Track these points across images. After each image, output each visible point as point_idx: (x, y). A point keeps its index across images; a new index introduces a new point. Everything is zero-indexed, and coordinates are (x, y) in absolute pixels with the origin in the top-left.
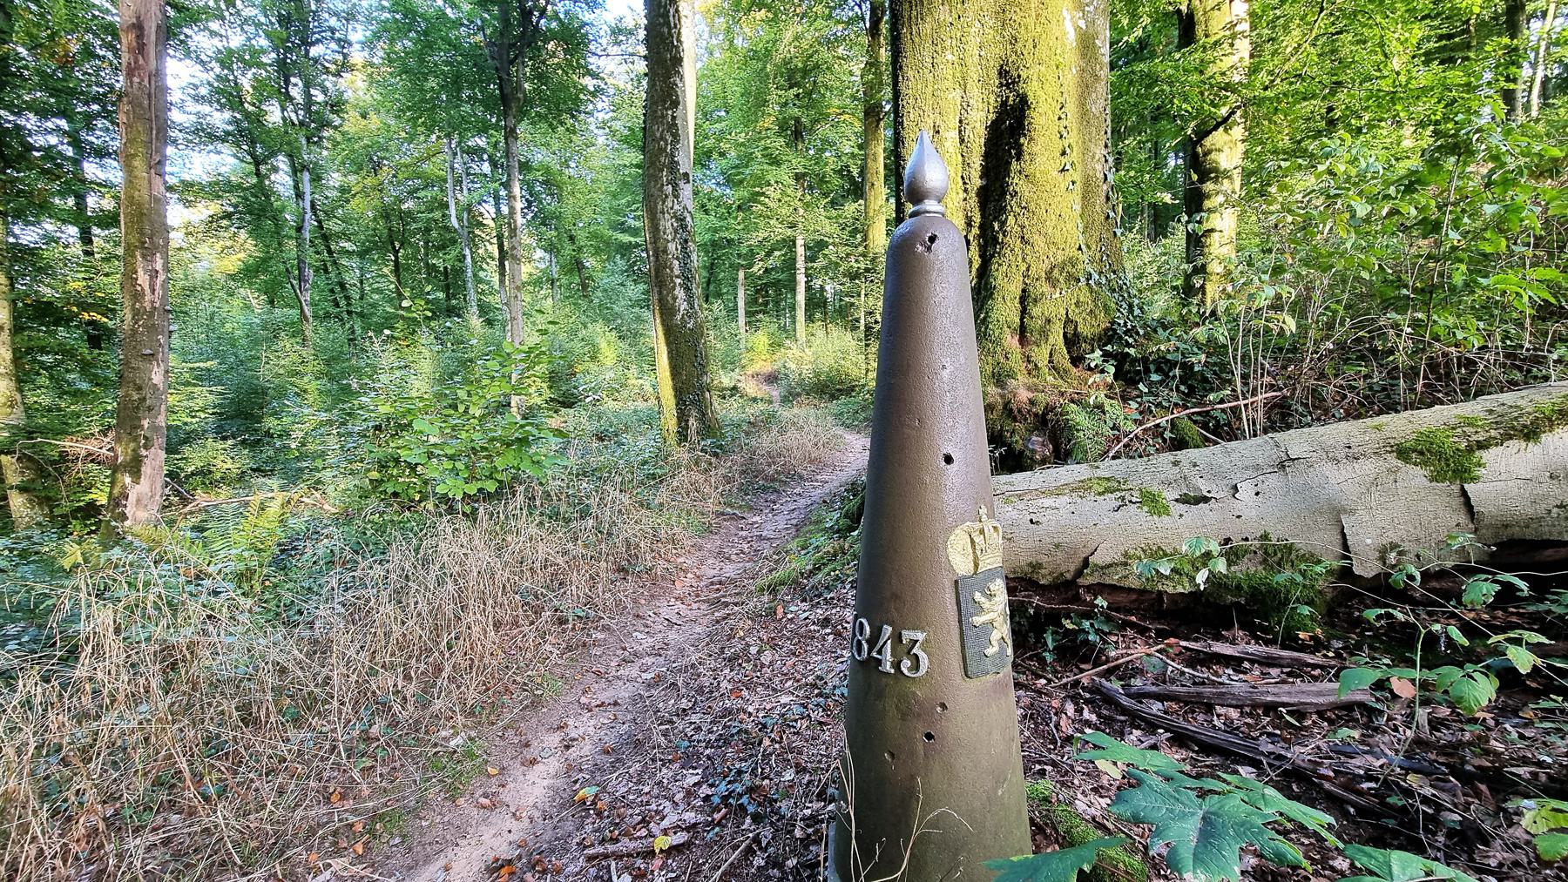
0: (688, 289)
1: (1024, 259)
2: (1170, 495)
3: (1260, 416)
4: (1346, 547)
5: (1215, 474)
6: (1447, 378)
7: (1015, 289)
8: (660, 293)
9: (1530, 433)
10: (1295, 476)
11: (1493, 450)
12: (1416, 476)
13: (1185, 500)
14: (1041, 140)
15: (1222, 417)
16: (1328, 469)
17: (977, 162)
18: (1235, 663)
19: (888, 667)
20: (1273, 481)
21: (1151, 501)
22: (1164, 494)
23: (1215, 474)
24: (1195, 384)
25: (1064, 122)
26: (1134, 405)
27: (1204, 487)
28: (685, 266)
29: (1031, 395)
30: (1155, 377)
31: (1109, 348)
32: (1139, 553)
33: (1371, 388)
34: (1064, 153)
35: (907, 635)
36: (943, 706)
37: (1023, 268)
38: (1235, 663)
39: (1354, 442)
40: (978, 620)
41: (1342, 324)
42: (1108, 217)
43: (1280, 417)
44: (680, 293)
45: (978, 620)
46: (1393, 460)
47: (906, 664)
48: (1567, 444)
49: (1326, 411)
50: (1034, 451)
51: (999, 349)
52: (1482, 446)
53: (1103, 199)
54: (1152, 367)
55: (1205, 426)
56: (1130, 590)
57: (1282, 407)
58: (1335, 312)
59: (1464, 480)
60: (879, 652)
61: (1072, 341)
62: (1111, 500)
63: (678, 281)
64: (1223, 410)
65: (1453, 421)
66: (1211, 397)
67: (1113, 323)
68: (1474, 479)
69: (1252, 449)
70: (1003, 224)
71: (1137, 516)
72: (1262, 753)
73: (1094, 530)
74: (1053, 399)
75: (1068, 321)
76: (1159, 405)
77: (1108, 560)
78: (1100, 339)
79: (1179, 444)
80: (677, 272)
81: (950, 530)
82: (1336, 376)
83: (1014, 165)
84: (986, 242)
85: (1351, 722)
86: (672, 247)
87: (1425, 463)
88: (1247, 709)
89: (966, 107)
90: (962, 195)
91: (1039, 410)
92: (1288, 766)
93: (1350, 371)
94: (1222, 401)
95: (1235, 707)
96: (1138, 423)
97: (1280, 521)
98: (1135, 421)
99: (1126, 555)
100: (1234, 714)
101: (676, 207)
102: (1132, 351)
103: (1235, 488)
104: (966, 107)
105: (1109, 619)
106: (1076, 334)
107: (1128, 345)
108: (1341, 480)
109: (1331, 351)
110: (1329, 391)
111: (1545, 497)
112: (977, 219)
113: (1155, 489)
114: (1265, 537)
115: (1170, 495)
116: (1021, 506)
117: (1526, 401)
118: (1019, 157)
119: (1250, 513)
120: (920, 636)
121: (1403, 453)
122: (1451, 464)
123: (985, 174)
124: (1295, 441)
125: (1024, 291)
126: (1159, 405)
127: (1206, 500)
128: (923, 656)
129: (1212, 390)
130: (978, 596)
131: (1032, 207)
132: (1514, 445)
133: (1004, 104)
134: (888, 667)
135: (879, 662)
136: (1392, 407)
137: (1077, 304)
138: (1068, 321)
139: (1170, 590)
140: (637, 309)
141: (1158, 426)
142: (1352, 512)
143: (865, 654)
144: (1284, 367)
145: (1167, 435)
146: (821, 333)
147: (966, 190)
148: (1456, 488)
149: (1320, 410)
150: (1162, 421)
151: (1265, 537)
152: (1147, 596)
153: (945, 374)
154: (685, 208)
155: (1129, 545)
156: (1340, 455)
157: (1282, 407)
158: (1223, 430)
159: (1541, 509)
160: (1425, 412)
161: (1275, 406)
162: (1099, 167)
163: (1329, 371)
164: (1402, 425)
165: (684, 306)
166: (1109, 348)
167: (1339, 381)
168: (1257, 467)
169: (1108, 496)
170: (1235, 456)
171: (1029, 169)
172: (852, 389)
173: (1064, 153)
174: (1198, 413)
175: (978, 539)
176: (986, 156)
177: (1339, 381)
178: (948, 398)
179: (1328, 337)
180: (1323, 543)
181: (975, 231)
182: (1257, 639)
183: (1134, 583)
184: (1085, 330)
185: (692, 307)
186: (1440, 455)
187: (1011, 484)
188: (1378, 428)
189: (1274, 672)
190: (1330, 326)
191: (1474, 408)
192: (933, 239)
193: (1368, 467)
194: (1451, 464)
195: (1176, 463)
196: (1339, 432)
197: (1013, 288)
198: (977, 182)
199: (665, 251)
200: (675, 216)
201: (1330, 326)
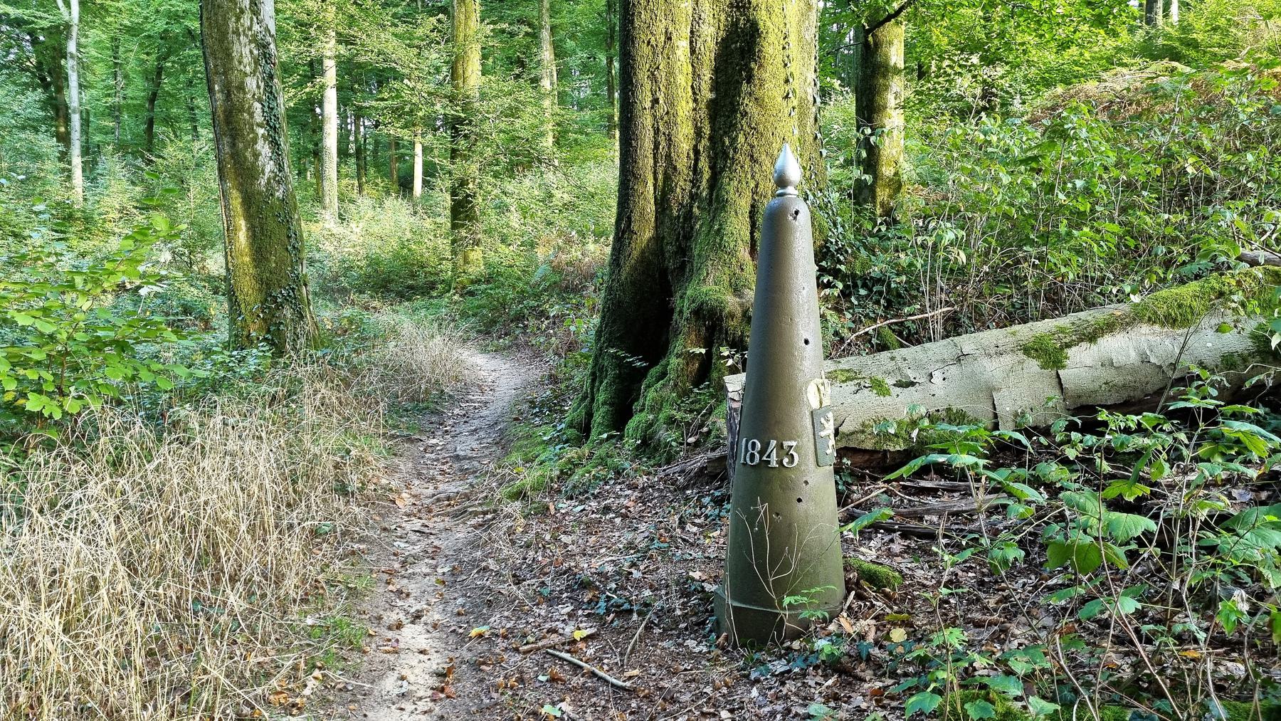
0: (275, 144)
1: (753, 177)
2: (890, 381)
3: (939, 328)
4: (996, 416)
5: (919, 366)
6: (1056, 302)
7: (744, 204)
8: (233, 145)
9: (1092, 338)
10: (967, 367)
11: (1074, 349)
12: (1033, 365)
13: (899, 384)
14: (769, 68)
15: (913, 327)
16: (985, 362)
17: (707, 75)
18: (932, 492)
19: (774, 464)
20: (954, 370)
21: (878, 386)
22: (887, 381)
23: (919, 366)
24: (894, 301)
25: (787, 52)
26: (849, 316)
27: (911, 375)
28: (270, 110)
30: (863, 292)
31: (824, 263)
32: (872, 423)
33: (1013, 306)
34: (787, 81)
35: (786, 444)
37: (752, 185)
38: (932, 492)
39: (1000, 343)
40: (823, 434)
41: (995, 252)
42: (816, 137)
43: (953, 326)
44: (264, 148)
45: (823, 434)
46: (1020, 353)
47: (786, 460)
49: (983, 324)
51: (734, 260)
52: (1068, 346)
53: (812, 120)
54: (859, 283)
55: (900, 334)
56: (865, 451)
57: (954, 319)
58: (990, 244)
59: (1058, 368)
60: (769, 456)
62: (851, 386)
63: (261, 131)
64: (913, 321)
65: (1054, 330)
66: (906, 310)
67: (827, 241)
68: (1063, 367)
69: (939, 349)
70: (734, 140)
71: (869, 396)
73: (841, 408)
76: (867, 316)
77: (852, 429)
79: (883, 347)
80: (259, 118)
81: (807, 383)
82: (991, 295)
83: (744, 86)
84: (716, 154)
85: (998, 513)
86: (251, 83)
87: (1038, 357)
89: (697, 19)
90: (691, 105)
93: (1000, 290)
94: (913, 314)
96: (853, 331)
97: (959, 396)
98: (850, 329)
99: (863, 425)
101: (256, 27)
102: (843, 268)
103: (931, 375)
104: (697, 19)
105: (852, 474)
107: (840, 262)
108: (993, 369)
109: (987, 273)
110: (986, 307)
111: (1099, 378)
112: (707, 131)
113: (880, 377)
114: (949, 410)
115: (890, 381)
117: (1088, 316)
118: (749, 79)
119: (940, 393)
120: (794, 444)
121: (1027, 351)
122: (1050, 356)
123: (715, 87)
124: (967, 342)
125: (753, 206)
126: (867, 316)
127: (913, 384)
129: (904, 304)
130: (823, 420)
131: (761, 128)
132: (1084, 345)
133: (735, 24)
134: (774, 464)
136: (1024, 321)
139: (892, 449)
140: (29, 135)
141: (866, 333)
142: (999, 390)
143: (757, 460)
144: (955, 287)
145: (874, 341)
146: (365, 203)
147: (695, 101)
148: (1054, 372)
149: (980, 321)
150: (870, 330)
151: (949, 410)
152: (876, 456)
153: (804, 292)
154: (267, 30)
155: (864, 418)
156: (993, 351)
157: (954, 319)
158: (912, 337)
159: (1097, 385)
160: (1039, 324)
161: (949, 319)
162: (810, 91)
163: (986, 292)
164: (1026, 332)
165: (270, 167)
166: (824, 263)
167: (992, 300)
168: (944, 361)
169: (849, 383)
170: (930, 353)
171: (759, 93)
172: (432, 286)
173: (787, 81)
174: (896, 324)
175: (822, 388)
176: (716, 71)
177: (992, 300)
178: (806, 307)
179: (985, 263)
180: (981, 409)
181: (705, 142)
182: (946, 479)
183: (868, 445)
185: (281, 169)
186: (1046, 351)
188: (1014, 334)
189: (956, 494)
190: (987, 254)
191: (1064, 322)
192: (797, 213)
193: (1008, 360)
194: (1050, 356)
195: (893, 359)
196: (992, 336)
197: (743, 202)
198: (707, 94)
199: (241, 87)
200: (254, 40)
201: (987, 254)
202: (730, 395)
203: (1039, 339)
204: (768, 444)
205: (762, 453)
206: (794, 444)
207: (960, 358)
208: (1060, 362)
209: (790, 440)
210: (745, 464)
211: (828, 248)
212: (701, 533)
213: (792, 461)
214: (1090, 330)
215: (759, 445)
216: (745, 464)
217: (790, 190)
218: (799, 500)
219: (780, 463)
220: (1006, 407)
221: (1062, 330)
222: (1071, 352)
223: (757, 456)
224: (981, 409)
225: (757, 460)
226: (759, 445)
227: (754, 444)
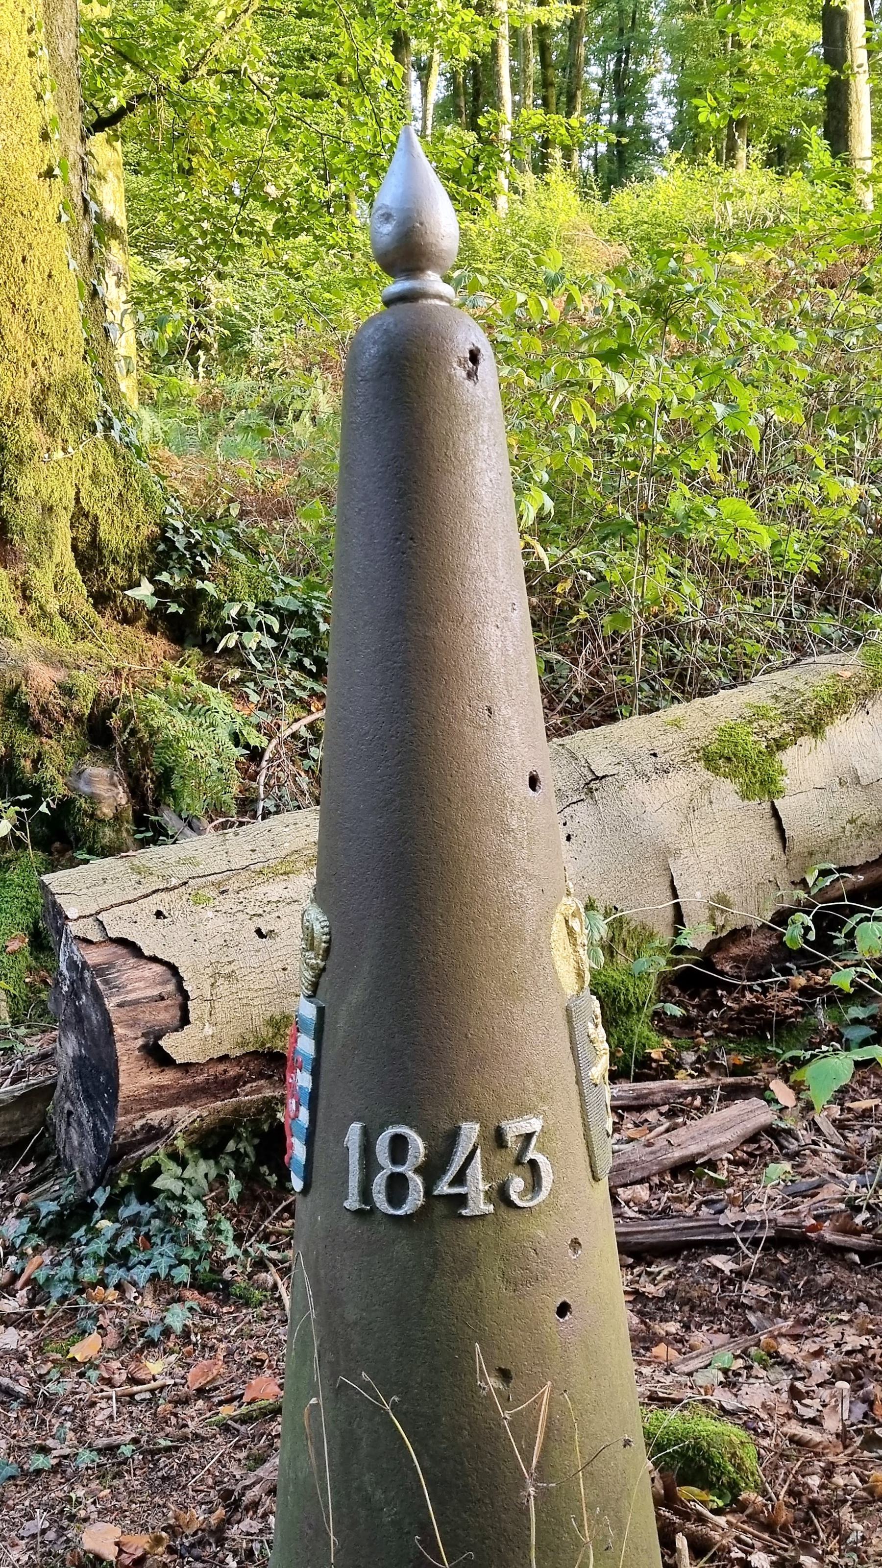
9: (815, 727)
11: (792, 751)
12: (727, 789)
16: (638, 790)
19: (479, 1204)
20: (583, 813)
29: (60, 675)
31: (164, 577)
35: (514, 1129)
36: (576, 1244)
39: (658, 746)
47: (517, 1185)
48: (851, 736)
50: (93, 798)
52: (779, 745)
60: (460, 1179)
61: (89, 556)
72: (727, 1229)
74: (106, 684)
75: (80, 514)
78: (143, 558)
87: (731, 775)
88: (656, 1180)
91: (83, 706)
92: (766, 1234)
95: (641, 1181)
100: (642, 1192)
106: (95, 543)
111: (839, 810)
116: (228, 903)
121: (710, 760)
122: (747, 765)
128: (541, 1159)
132: (806, 741)
135: (461, 1200)
137: (95, 477)
138: (80, 514)
143: (415, 1198)
148: (767, 805)
166: (164, 577)
184: (112, 535)
187: (190, 861)
188: (676, 724)
189: (651, 1116)
193: (681, 784)
202: (74, 928)
203: (727, 734)
204: (453, 1136)
205: (431, 1171)
206: (535, 1125)
207: (592, 784)
208: (773, 781)
209: (523, 1111)
210: (366, 1213)
211: (170, 543)
212: (39, 1348)
213: (535, 1183)
214: (810, 709)
215: (418, 1146)
216: (366, 1213)
217: (432, 281)
218: (563, 1309)
219: (501, 1196)
220: (695, 898)
221: (759, 713)
222: (788, 758)
223: (417, 1182)
224: (654, 910)
225: (415, 1198)
226: (418, 1146)
227: (399, 1146)
